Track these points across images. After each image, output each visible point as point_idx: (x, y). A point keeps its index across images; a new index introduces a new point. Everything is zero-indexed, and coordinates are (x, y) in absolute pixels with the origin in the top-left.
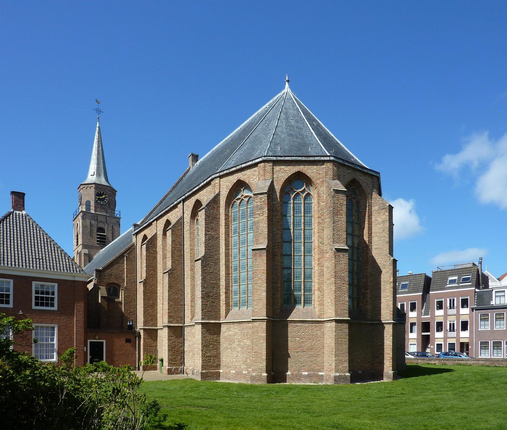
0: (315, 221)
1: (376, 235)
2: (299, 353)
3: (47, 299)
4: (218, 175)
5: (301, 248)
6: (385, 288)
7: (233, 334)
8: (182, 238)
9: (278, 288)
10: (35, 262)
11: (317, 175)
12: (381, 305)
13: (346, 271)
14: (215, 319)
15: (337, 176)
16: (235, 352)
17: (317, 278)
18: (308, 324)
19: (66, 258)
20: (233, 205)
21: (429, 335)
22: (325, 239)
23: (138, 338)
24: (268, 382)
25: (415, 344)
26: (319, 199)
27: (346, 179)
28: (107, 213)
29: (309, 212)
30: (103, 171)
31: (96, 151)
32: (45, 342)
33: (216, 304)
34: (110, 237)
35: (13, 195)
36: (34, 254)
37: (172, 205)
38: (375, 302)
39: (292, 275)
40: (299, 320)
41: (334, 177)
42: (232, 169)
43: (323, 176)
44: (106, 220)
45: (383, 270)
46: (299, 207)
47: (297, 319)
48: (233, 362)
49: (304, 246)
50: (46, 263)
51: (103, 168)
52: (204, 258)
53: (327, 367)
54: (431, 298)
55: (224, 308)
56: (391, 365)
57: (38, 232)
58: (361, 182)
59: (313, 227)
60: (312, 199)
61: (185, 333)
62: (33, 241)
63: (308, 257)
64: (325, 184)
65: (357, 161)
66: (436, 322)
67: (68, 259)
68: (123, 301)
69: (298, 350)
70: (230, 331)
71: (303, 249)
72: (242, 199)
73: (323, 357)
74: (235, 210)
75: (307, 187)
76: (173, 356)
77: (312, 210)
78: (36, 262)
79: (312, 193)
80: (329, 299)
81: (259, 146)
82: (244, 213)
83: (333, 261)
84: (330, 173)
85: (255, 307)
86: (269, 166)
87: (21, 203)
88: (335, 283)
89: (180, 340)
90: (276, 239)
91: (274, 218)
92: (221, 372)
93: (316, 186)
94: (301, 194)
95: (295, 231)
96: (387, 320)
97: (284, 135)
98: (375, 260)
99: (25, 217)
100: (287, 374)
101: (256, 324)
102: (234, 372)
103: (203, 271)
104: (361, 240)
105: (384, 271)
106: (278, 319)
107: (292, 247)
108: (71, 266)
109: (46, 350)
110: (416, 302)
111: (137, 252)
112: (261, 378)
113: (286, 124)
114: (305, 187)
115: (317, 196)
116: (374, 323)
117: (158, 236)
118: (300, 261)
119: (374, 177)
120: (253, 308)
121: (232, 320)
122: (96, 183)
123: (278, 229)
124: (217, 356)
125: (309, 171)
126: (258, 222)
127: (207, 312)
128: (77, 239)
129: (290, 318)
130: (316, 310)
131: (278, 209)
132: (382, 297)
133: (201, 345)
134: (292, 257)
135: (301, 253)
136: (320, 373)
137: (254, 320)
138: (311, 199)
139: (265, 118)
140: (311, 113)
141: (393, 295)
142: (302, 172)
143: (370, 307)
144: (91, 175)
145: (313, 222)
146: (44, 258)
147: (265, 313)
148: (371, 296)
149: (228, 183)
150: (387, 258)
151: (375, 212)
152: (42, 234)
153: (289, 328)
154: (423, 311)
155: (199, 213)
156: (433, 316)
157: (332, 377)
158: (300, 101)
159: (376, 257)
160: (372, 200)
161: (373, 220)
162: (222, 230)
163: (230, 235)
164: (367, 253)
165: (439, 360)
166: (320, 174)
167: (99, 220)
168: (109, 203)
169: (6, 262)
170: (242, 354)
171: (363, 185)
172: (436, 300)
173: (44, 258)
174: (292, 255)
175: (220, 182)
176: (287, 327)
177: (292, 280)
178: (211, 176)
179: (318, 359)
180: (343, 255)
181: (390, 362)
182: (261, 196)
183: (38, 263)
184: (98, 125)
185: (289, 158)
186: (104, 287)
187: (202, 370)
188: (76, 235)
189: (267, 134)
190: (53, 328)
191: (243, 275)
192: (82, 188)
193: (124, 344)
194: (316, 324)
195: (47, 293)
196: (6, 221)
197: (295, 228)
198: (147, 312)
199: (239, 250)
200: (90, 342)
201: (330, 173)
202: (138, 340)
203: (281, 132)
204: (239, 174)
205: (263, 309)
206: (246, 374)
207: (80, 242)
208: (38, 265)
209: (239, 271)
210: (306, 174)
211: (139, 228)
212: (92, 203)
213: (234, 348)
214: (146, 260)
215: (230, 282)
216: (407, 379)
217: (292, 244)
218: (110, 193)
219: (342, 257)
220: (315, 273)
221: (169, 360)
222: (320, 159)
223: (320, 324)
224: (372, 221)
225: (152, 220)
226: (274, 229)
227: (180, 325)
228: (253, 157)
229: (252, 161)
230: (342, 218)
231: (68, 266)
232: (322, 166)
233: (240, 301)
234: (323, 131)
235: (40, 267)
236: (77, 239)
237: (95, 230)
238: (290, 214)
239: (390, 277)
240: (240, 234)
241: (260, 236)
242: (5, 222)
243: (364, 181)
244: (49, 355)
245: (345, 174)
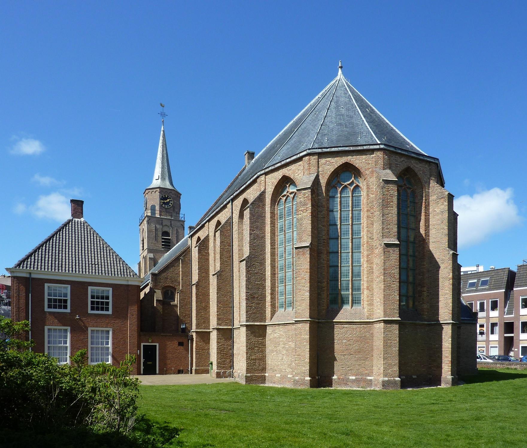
0: (364, 215)
1: (434, 227)
3: (102, 303)
4: (263, 172)
5: (349, 245)
6: (443, 285)
8: (231, 238)
9: (324, 287)
10: (90, 268)
11: (366, 165)
12: (439, 303)
13: (397, 268)
14: (260, 321)
15: (389, 165)
16: (280, 354)
17: (366, 276)
18: (356, 325)
19: (121, 263)
20: (278, 202)
21: (513, 337)
22: (374, 234)
23: (191, 341)
24: (312, 386)
25: (497, 347)
26: (369, 191)
27: (398, 168)
28: (171, 216)
29: (358, 205)
30: (167, 175)
31: (161, 155)
32: (100, 346)
33: (261, 305)
34: (174, 240)
35: (72, 203)
36: (90, 260)
37: (222, 205)
38: (433, 300)
39: (339, 273)
40: (346, 321)
41: (385, 166)
42: (277, 165)
43: (373, 166)
44: (171, 224)
45: (441, 265)
46: (346, 201)
47: (344, 320)
49: (352, 242)
50: (102, 268)
51: (168, 171)
52: (248, 258)
53: (376, 371)
54: (515, 295)
55: (270, 310)
56: (450, 370)
57: (95, 238)
58: (416, 170)
59: (362, 221)
60: (361, 191)
61: (234, 335)
62: (67, 247)
63: (357, 254)
64: (375, 175)
65: (414, 147)
66: (520, 322)
67: (123, 264)
68: (179, 304)
69: (345, 353)
71: (350, 246)
72: (288, 196)
73: (372, 360)
74: (281, 208)
75: (355, 178)
76: (221, 359)
77: (361, 204)
78: (92, 267)
79: (361, 185)
80: (378, 298)
81: (306, 138)
82: (290, 210)
83: (382, 257)
84: (380, 162)
86: (314, 159)
87: (80, 211)
88: (384, 281)
89: (229, 343)
91: (320, 214)
92: (267, 376)
93: (365, 177)
94: (349, 187)
95: (342, 227)
96: (446, 320)
97: (333, 125)
98: (433, 255)
99: (83, 224)
100: (333, 378)
101: (299, 325)
103: (248, 272)
104: (417, 234)
105: (442, 266)
106: (323, 321)
107: (339, 244)
108: (125, 271)
109: (102, 353)
110: (498, 299)
111: (192, 255)
112: (304, 382)
113: (336, 113)
114: (353, 178)
115: (366, 187)
116: (431, 324)
117: (210, 237)
118: (348, 259)
119: (431, 164)
120: (296, 309)
121: (277, 322)
122: (160, 187)
123: (323, 226)
124: (263, 359)
125: (357, 161)
126: (301, 219)
127: (251, 314)
128: (143, 244)
129: (337, 320)
130: (365, 310)
131: (323, 204)
132: (440, 295)
133: (246, 348)
134: (339, 254)
135: (349, 250)
136: (369, 378)
137: (297, 322)
138: (360, 192)
139: (316, 108)
140: (364, 100)
141: (452, 293)
143: (427, 306)
144: (156, 180)
145: (362, 216)
146: (100, 263)
147: (308, 314)
148: (428, 294)
149: (274, 179)
150: (445, 252)
151: (433, 202)
152: (98, 240)
153: (335, 330)
154: (506, 309)
155: (245, 212)
156: (518, 315)
157: (380, 381)
158: (353, 88)
159: (433, 252)
160: (429, 190)
161: (430, 210)
162: (268, 228)
163: (276, 234)
164: (424, 248)
165: (521, 364)
167: (164, 224)
168: (173, 207)
169: (64, 269)
170: (287, 357)
172: (521, 298)
173: (100, 263)
174: (339, 252)
175: (265, 179)
176: (333, 328)
177: (339, 278)
178: (256, 173)
179: (367, 363)
180: (393, 250)
181: (448, 366)
182: (304, 192)
183: (94, 268)
184: (162, 129)
185: (335, 149)
186: (160, 290)
187: (246, 374)
188: (142, 240)
189: (316, 125)
190: (108, 332)
191: (289, 274)
192: (147, 193)
193: (177, 347)
194: (365, 325)
195: (102, 298)
196: (66, 229)
197: (343, 224)
198: (200, 315)
199: (285, 249)
201: (381, 162)
202: (191, 343)
203: (330, 122)
204: (284, 169)
205: (306, 310)
206: (290, 378)
207: (146, 247)
208: (94, 271)
209: (285, 271)
210: (354, 164)
211: (193, 230)
212: (157, 208)
213: (279, 351)
214: (199, 262)
215: (275, 282)
216: (469, 384)
217: (339, 240)
218: (175, 196)
219: (392, 252)
220: (364, 271)
221: (218, 363)
222: (369, 147)
223: (369, 326)
224: (429, 212)
225: (204, 222)
226: (320, 225)
227: (230, 327)
228: (298, 151)
229: (296, 156)
230: (393, 210)
231: (122, 271)
232: (371, 156)
233: (285, 302)
234: (377, 118)
235: (95, 272)
236: (143, 244)
237: (160, 234)
238: (337, 209)
239: (449, 273)
240: (286, 232)
241: (304, 233)
242: (64, 230)
243: (421, 169)
244: (104, 358)
245: (397, 163)
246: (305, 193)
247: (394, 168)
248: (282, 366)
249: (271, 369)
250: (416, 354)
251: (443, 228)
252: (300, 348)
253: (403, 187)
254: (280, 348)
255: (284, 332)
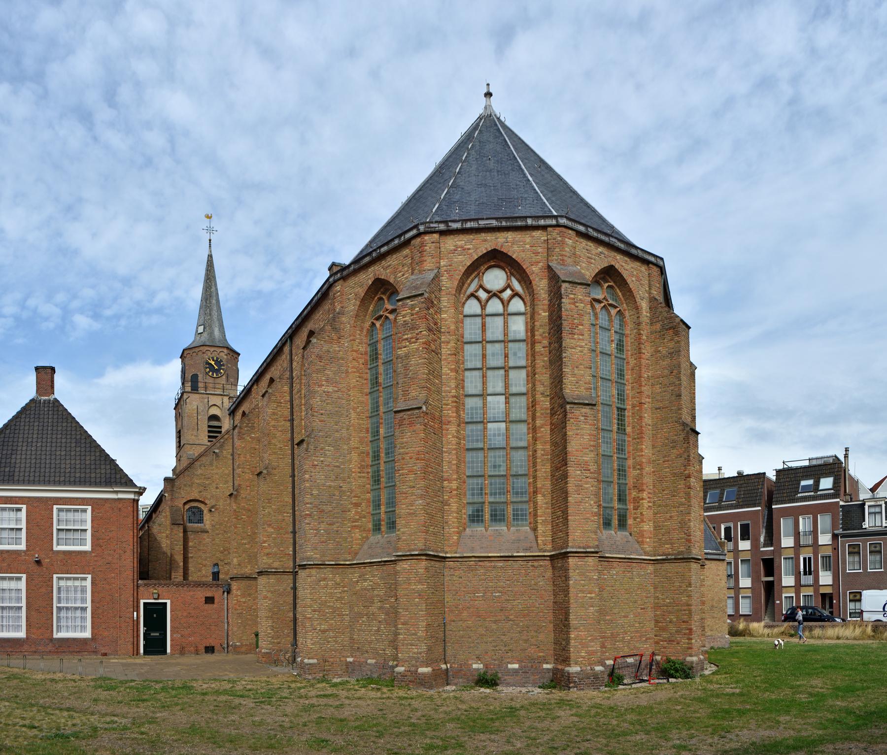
2: (500, 624)
6: (675, 489)
7: (370, 587)
27: (592, 265)
48: (370, 642)
70: (365, 580)
85: (402, 530)
90: (448, 389)
102: (373, 661)
142: (502, 250)
143: (648, 526)
148: (650, 504)
166: (539, 253)
171: (629, 281)
200: (144, 603)
210: (509, 254)
226: (445, 369)
230: (583, 340)
241: (411, 383)
245: (590, 255)
246: (412, 305)
247: (585, 265)
248: (378, 644)
249: (358, 648)
250: (632, 616)
251: (672, 384)
252: (407, 609)
253: (603, 302)
254: (373, 609)
255: (381, 578)
